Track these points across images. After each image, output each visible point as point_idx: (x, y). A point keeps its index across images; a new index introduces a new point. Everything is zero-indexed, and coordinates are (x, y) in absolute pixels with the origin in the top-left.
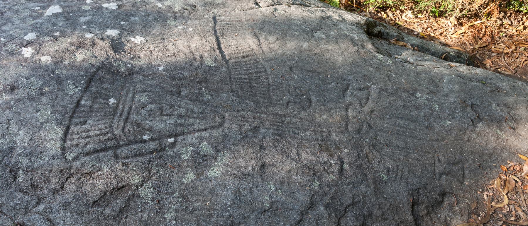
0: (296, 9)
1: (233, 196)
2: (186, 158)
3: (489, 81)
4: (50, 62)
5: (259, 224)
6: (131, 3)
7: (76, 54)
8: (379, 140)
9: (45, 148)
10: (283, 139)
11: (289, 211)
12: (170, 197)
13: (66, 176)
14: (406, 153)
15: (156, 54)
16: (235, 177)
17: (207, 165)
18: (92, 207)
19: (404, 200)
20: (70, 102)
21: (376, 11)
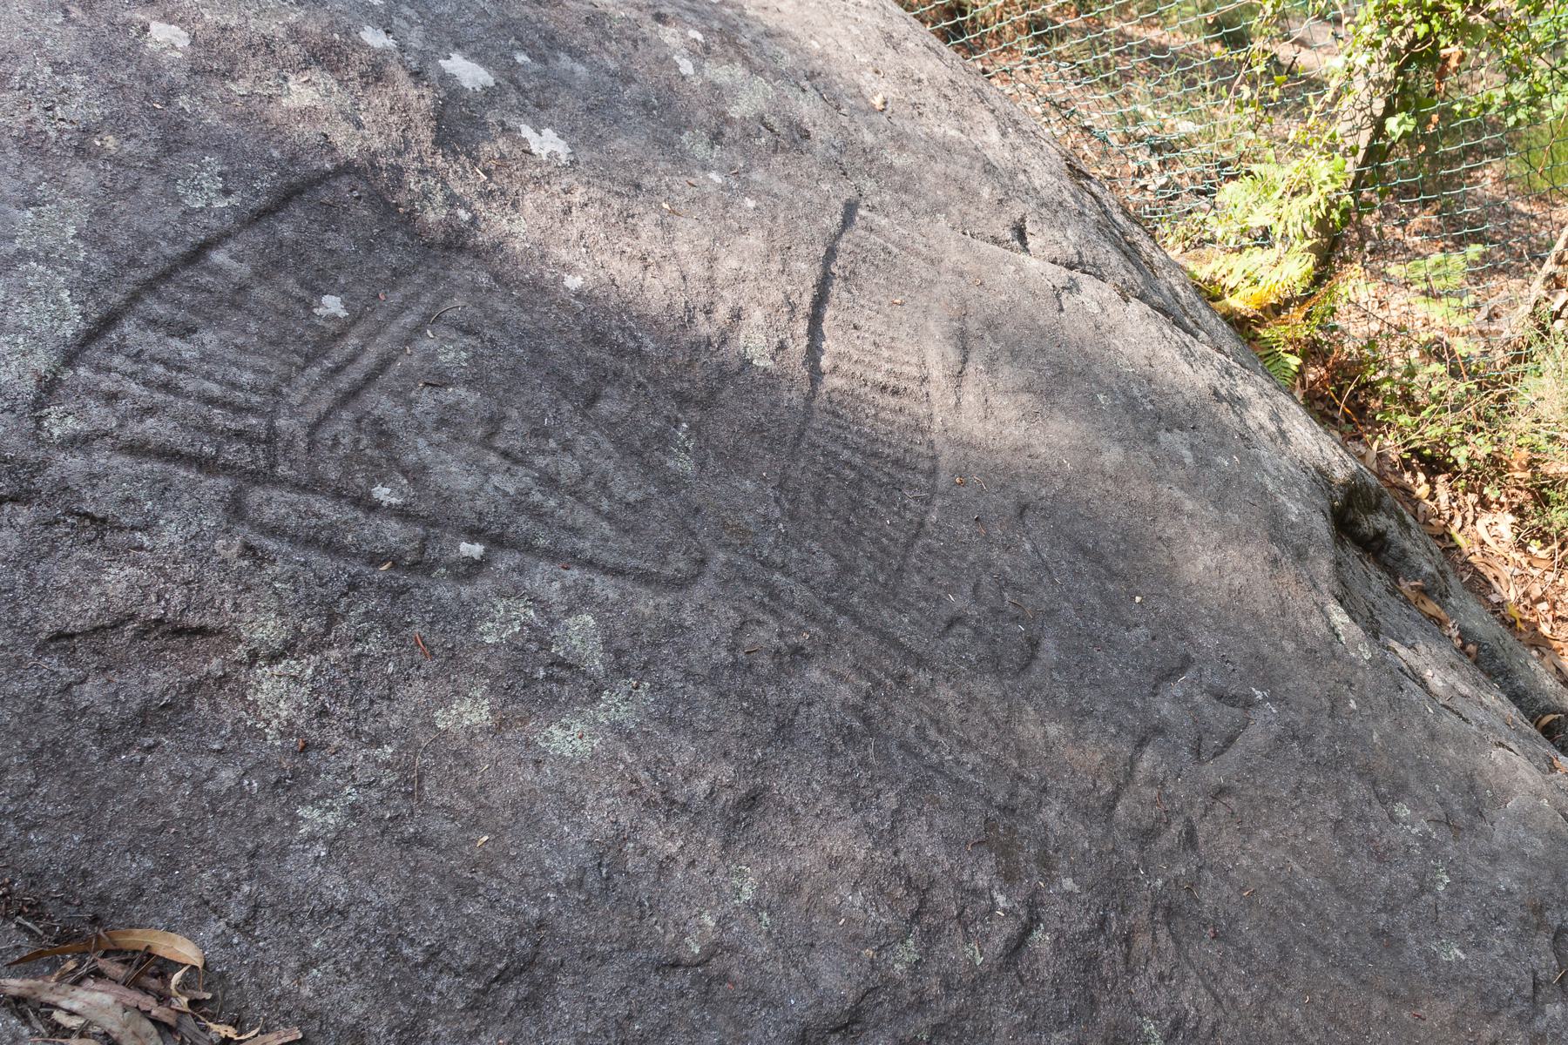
0: (1142, 319)
1: (588, 855)
2: (489, 640)
4: (180, 55)
7: (292, 78)
8: (1197, 901)
14: (1266, 991)
16: (631, 793)
18: (41, 649)
21: (1404, 460)
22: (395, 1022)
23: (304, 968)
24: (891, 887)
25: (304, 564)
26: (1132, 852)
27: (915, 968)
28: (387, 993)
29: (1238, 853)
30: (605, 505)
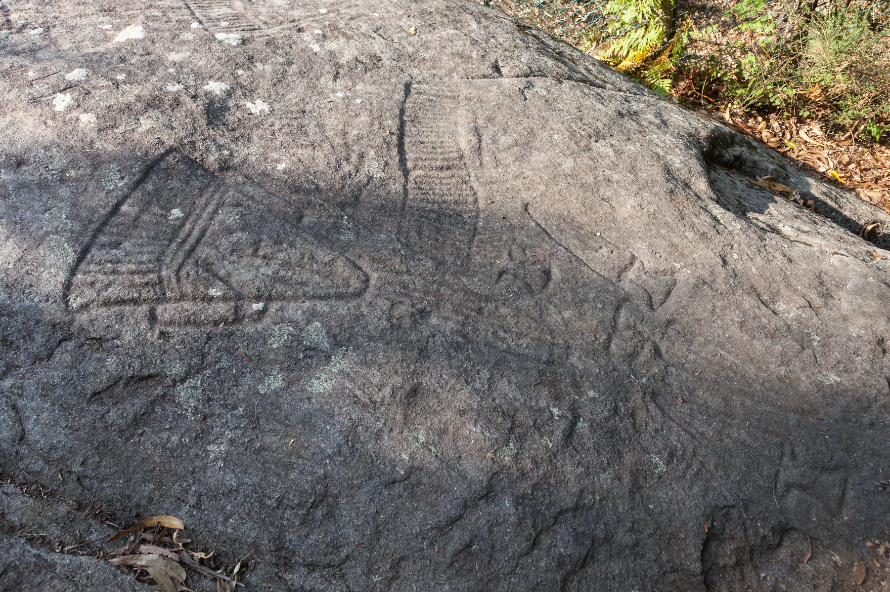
0: (571, 89)
1: (341, 438)
2: (275, 346)
4: (93, 125)
5: (376, 506)
6: (266, 38)
7: (141, 118)
8: (669, 385)
10: (470, 346)
11: (442, 493)
12: (227, 413)
13: (59, 335)
14: (721, 425)
15: (280, 139)
16: (355, 403)
18: (89, 402)
19: (690, 524)
20: (103, 204)
21: (747, 113)
22: (271, 537)
23: (226, 519)
24: (495, 418)
25: (186, 334)
27: (516, 457)
29: (687, 353)
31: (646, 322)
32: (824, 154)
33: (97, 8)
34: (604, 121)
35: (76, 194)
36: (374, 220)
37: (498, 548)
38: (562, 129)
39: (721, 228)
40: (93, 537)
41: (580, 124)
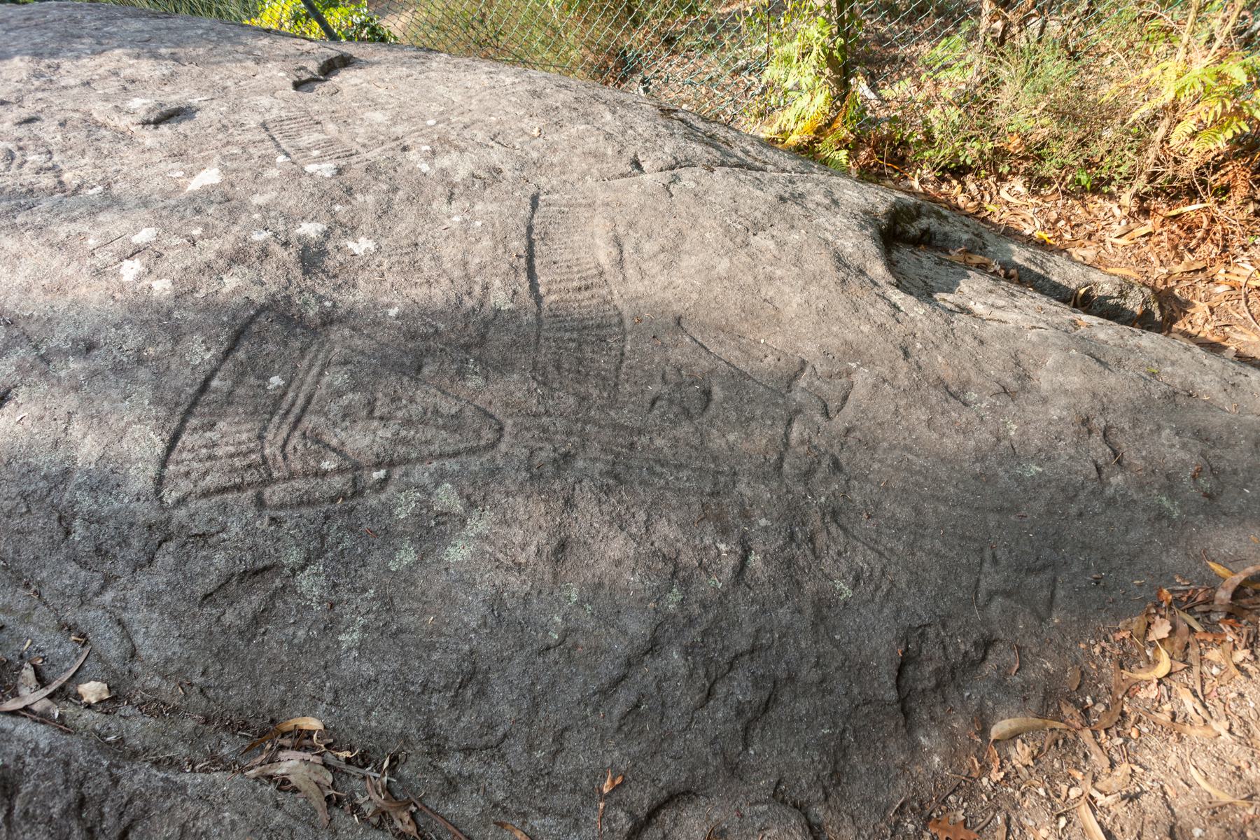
0: (724, 177)
2: (402, 517)
3: (1169, 369)
4: (168, 292)
7: (225, 277)
8: (851, 501)
9: (125, 476)
13: (158, 536)
14: (912, 537)
16: (497, 567)
17: (445, 534)
18: (201, 606)
19: (882, 651)
21: (939, 178)
23: (368, 713)
25: (300, 517)
26: (800, 488)
28: (410, 712)
30: (440, 421)
31: (823, 433)
32: (1029, 213)
33: (165, 154)
34: (763, 210)
35: (158, 375)
36: (504, 359)
37: (669, 704)
38: (715, 225)
39: (901, 316)
40: (225, 751)
41: (734, 217)
